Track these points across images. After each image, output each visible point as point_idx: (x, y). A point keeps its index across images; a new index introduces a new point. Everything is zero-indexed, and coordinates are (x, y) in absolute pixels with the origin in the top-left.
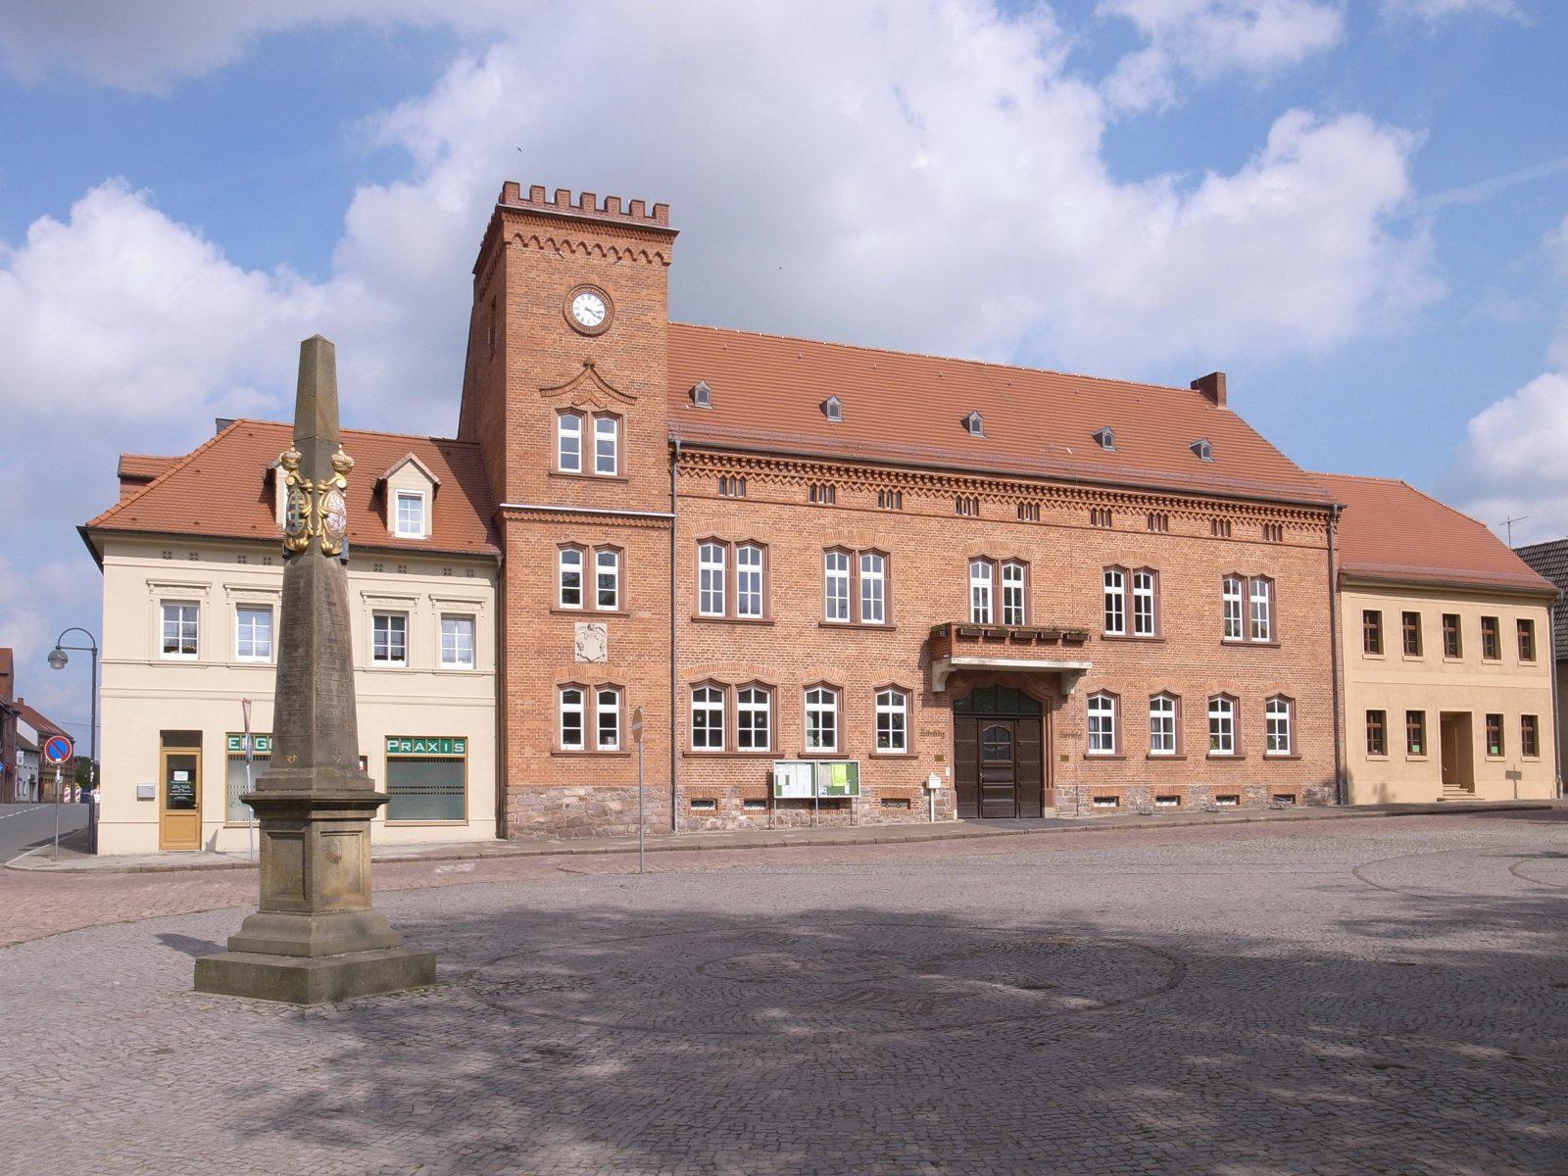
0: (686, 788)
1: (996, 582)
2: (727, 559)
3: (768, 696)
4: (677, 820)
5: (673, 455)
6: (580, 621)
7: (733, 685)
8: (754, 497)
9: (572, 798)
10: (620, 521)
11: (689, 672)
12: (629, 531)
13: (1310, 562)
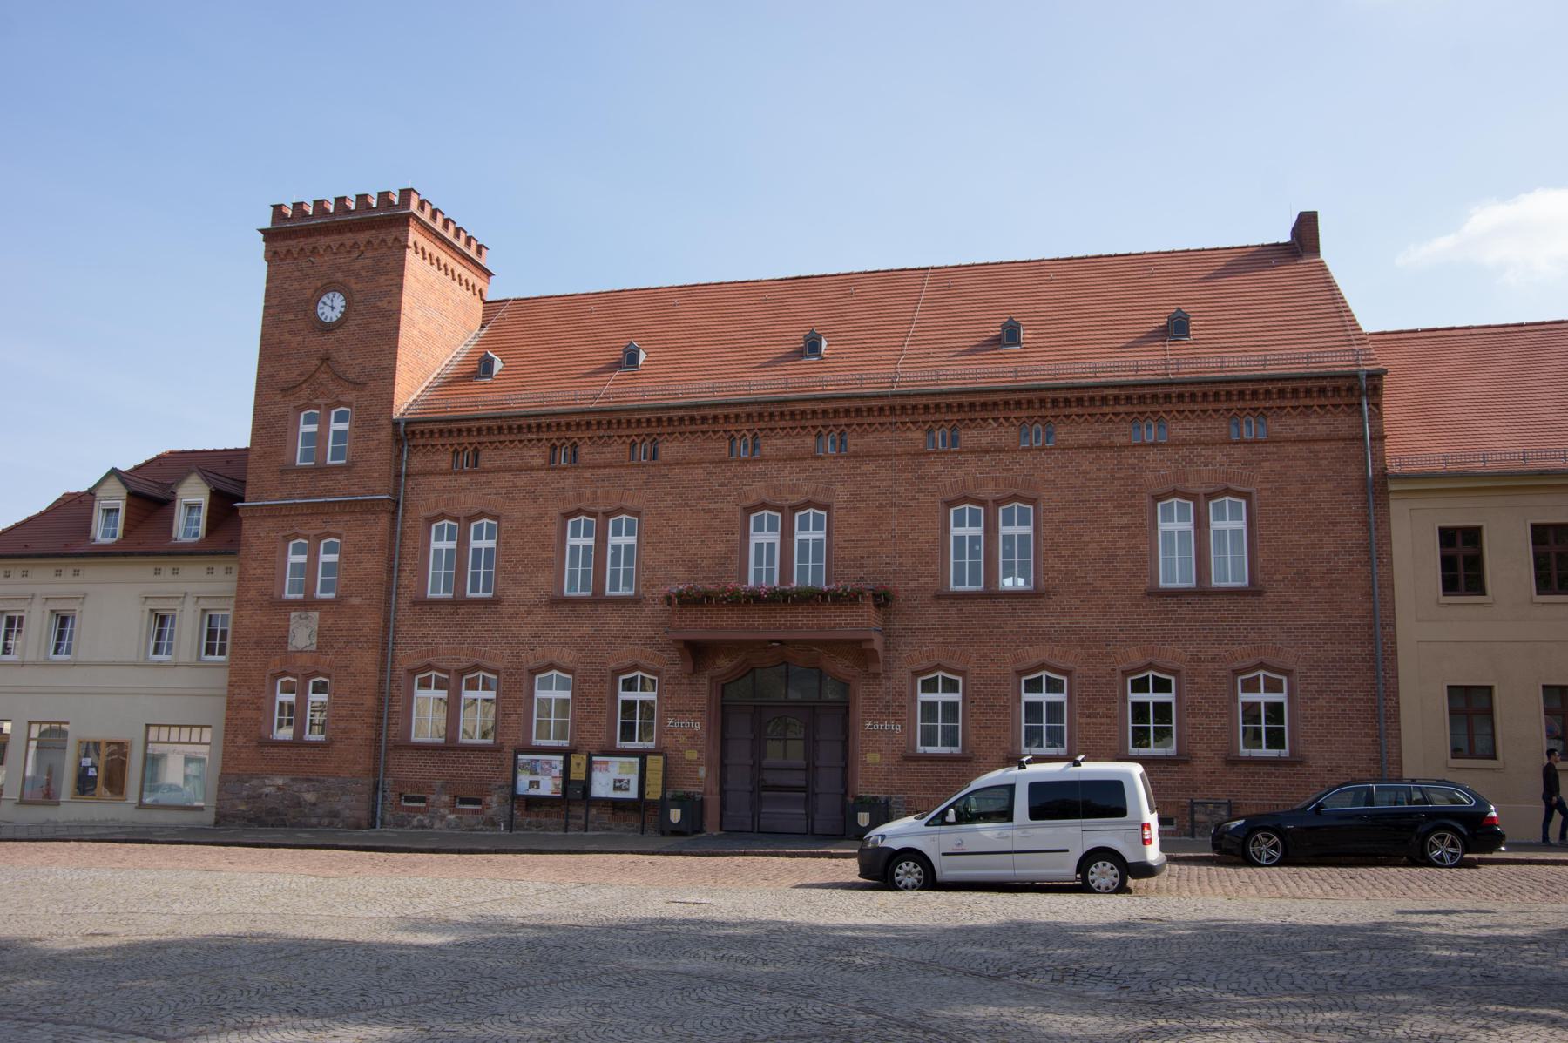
0: (395, 781)
2: (638, 533)
6: (295, 610)
7: (453, 671)
8: (488, 466)
9: (271, 788)
13: (1324, 462)
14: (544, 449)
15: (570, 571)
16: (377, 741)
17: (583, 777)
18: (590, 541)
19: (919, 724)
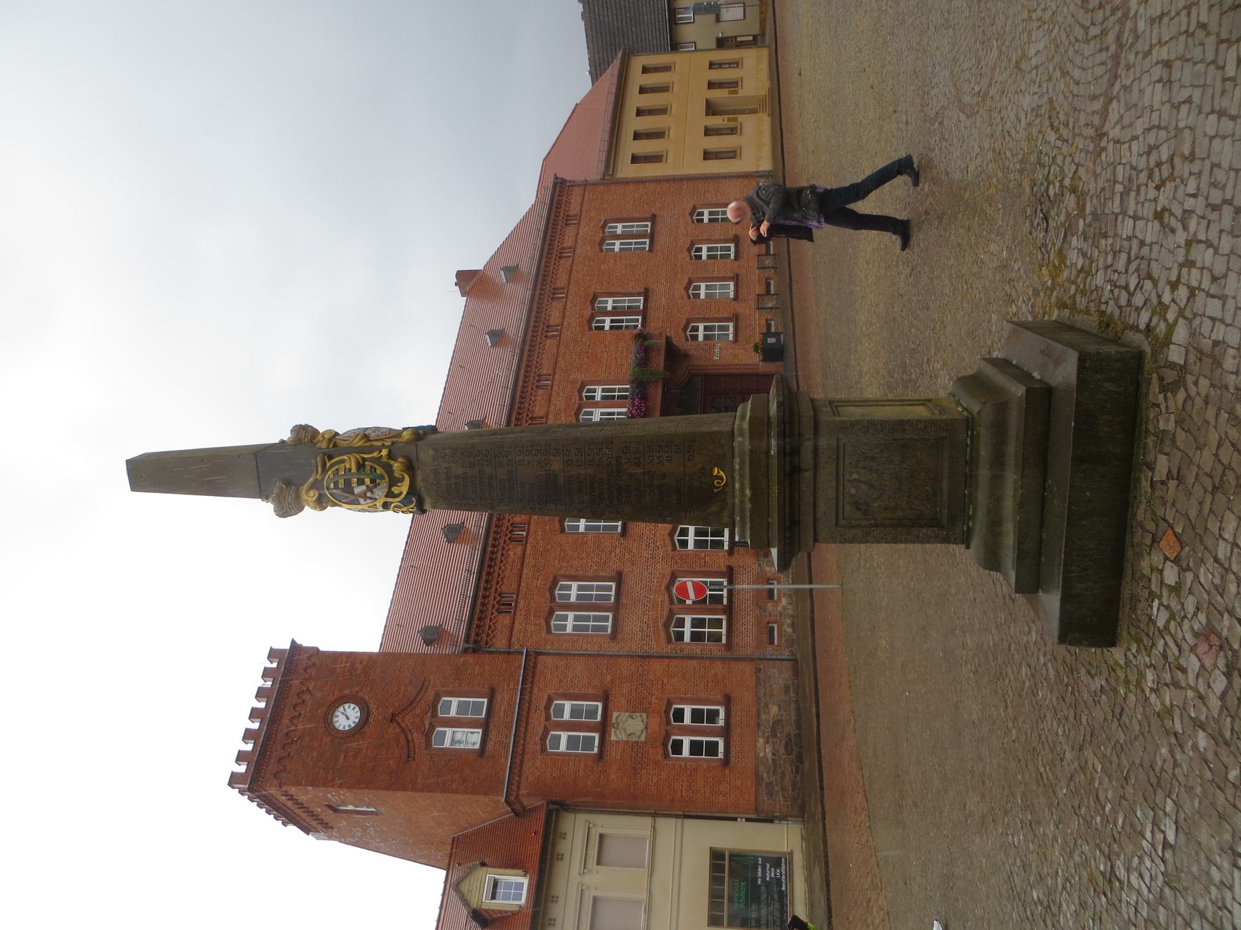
1: (597, 405)
4: (786, 657)
5: (475, 651)
9: (767, 750)
11: (658, 645)
12: (535, 690)
14: (511, 546)
16: (722, 659)
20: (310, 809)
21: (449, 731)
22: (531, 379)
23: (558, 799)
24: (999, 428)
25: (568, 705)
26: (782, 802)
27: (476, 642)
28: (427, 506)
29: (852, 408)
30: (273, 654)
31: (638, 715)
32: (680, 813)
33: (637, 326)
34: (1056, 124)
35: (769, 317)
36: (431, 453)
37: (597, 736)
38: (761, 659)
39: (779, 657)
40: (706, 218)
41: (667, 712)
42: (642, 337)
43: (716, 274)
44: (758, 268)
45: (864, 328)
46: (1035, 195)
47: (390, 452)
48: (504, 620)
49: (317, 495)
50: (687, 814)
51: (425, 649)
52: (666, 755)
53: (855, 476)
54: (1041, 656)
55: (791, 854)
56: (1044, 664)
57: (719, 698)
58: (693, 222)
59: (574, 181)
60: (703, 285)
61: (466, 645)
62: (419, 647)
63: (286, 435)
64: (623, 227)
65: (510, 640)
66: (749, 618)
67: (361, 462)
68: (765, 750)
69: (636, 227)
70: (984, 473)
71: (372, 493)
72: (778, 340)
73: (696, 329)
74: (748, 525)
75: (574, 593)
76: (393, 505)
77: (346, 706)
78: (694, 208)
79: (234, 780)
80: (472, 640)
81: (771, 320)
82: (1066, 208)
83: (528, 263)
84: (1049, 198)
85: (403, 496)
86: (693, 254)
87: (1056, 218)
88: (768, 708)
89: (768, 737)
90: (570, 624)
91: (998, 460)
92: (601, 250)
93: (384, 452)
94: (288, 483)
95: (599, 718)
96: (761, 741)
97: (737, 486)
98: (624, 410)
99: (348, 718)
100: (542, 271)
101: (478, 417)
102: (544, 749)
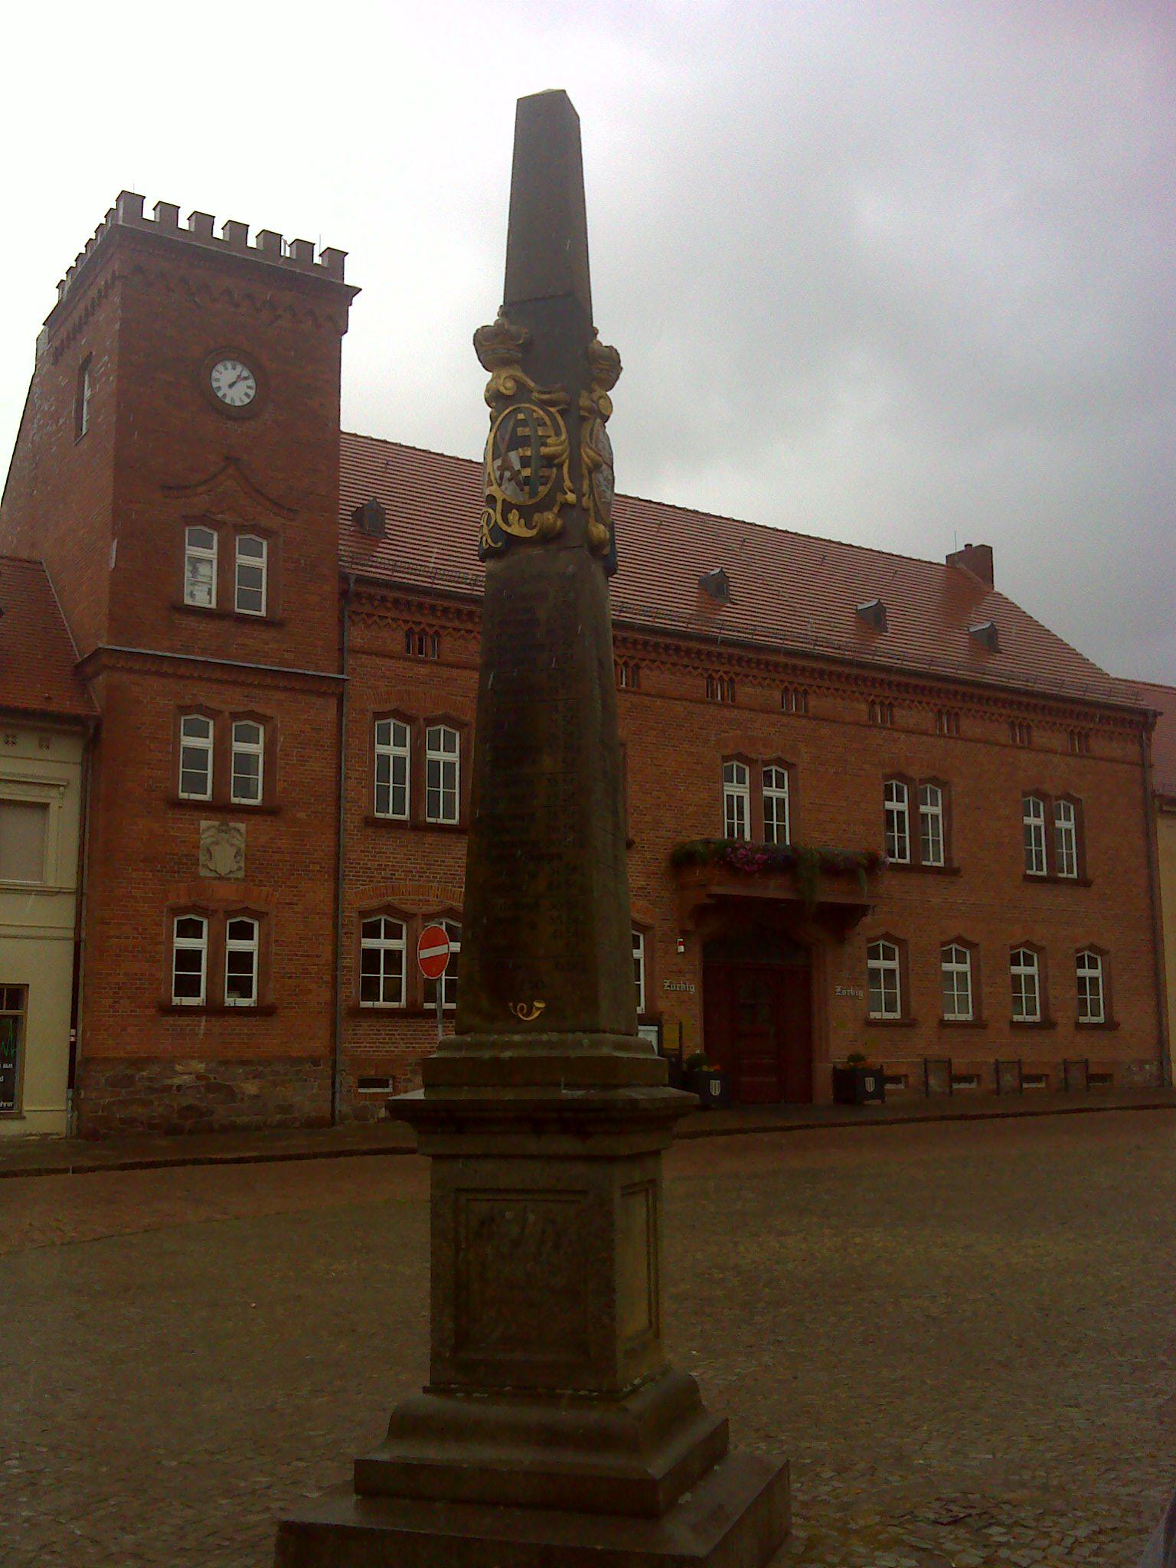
1: (755, 790)
3: (404, 928)
4: (337, 1106)
5: (344, 594)
10: (268, 681)
11: (357, 896)
12: (282, 696)
15: (1040, 845)
17: (677, 1046)
18: (431, 755)
19: (255, 975)
20: (66, 350)
21: (212, 554)
22: (801, 680)
23: (103, 735)
24: (601, 1440)
25: (256, 749)
26: (101, 1102)
27: (358, 595)
28: (488, 564)
29: (644, 1215)
30: (336, 257)
31: (242, 864)
32: (83, 936)
33: (893, 856)
34: (1102, 1538)
35: (911, 1079)
36: (571, 569)
37: (207, 797)
38: (334, 1068)
39: (337, 1095)
40: (1085, 972)
41: (246, 911)
42: (873, 864)
43: (986, 990)
44: (997, 1062)
45: (858, 1240)
46: (996, 1506)
47: (572, 506)
48: (395, 641)
49: (507, 392)
50: (82, 944)
51: (345, 519)
52: (176, 911)
53: (531, 1217)
54: (280, 1504)
55: (20, 1117)
56: (268, 1509)
57: (271, 998)
58: (1078, 951)
59: (1149, 746)
60: (965, 968)
61: (353, 579)
62: (350, 499)
63: (605, 338)
64: (1068, 831)
65: (364, 653)
66: (403, 1047)
67: (556, 461)
68: (187, 1073)
69: (1068, 851)
70: (530, 1414)
71: (510, 480)
72: (871, 1096)
73: (889, 957)
74: (457, 1055)
75: (441, 756)
76: (491, 511)
77: (251, 382)
78: (1102, 952)
79: (130, 201)
80: (362, 589)
81: (907, 1085)
82: (964, 1550)
83: (998, 669)
84: (985, 1527)
85: (504, 527)
86: (1022, 950)
87: (952, 1537)
88: (254, 1078)
89: (207, 1078)
90: (391, 750)
91: (551, 1437)
92: (1025, 794)
93: (571, 497)
94: (527, 347)
95: (235, 800)
96: (200, 1067)
97: (517, 1038)
98: (747, 837)
99: (231, 386)
100: (988, 693)
101: (734, 593)
102: (185, 710)
